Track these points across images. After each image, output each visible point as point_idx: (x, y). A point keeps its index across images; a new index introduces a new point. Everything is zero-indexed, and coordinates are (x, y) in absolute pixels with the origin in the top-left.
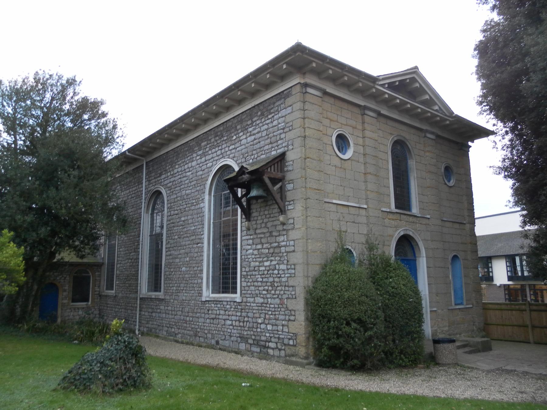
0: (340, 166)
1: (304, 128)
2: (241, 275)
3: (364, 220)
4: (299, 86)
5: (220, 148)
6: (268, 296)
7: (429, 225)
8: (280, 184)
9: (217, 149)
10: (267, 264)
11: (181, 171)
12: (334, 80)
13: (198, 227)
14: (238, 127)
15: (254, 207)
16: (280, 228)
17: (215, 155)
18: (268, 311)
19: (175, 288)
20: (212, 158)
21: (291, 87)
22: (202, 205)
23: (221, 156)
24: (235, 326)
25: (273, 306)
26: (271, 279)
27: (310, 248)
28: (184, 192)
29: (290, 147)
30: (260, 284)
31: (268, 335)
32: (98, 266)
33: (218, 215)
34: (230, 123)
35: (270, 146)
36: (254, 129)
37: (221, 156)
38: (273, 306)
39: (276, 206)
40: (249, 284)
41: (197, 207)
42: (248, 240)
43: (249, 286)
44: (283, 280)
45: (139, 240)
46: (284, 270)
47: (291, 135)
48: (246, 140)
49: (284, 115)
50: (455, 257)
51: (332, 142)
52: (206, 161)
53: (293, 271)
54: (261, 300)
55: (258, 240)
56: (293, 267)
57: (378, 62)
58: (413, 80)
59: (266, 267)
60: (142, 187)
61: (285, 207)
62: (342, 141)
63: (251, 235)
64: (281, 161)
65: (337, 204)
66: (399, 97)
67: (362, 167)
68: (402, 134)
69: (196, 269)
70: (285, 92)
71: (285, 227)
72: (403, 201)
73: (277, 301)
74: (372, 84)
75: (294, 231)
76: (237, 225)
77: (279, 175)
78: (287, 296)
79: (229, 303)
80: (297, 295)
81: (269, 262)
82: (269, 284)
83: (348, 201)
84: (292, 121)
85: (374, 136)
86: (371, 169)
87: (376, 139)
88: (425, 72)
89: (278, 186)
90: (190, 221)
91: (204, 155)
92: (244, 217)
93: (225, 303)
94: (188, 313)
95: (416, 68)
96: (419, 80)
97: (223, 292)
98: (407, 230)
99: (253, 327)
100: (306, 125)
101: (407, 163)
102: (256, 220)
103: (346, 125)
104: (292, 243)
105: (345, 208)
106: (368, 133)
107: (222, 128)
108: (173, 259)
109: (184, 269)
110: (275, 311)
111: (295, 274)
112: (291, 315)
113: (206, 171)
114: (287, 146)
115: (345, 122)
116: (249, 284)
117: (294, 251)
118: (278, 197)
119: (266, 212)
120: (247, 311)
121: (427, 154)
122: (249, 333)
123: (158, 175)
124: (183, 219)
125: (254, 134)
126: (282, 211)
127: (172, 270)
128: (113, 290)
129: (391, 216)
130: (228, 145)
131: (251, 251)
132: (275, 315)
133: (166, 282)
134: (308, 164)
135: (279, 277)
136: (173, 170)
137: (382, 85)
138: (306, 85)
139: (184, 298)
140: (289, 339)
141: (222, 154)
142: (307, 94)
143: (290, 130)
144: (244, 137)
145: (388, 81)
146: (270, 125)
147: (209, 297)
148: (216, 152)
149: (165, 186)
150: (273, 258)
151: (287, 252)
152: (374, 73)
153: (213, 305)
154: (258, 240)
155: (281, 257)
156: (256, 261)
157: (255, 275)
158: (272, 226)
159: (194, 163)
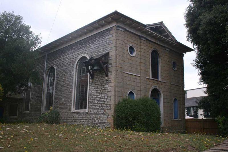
1: (117, 43)
2: (89, 101)
3: (139, 81)
4: (115, 27)
5: (82, 49)
6: (100, 109)
7: (165, 85)
8: (106, 65)
9: (80, 50)
10: (99, 96)
11: (64, 58)
12: (129, 25)
13: (71, 82)
14: (90, 41)
15: (95, 73)
16: (106, 82)
17: (79, 52)
18: (99, 115)
19: (58, 108)
20: (78, 53)
21: (112, 27)
22: (72, 73)
23: (82, 53)
24: (85, 122)
25: (101, 113)
26: (101, 102)
27: (117, 90)
28: (64, 68)
29: (111, 50)
30: (96, 104)
31: (99, 124)
32: (22, 100)
33: (79, 77)
34: (86, 40)
35: (103, 49)
36: (97, 43)
37: (82, 53)
38: (101, 113)
39: (104, 73)
40: (92, 105)
41: (70, 74)
42: (92, 87)
43: (92, 106)
44: (106, 102)
45: (42, 88)
46: (106, 99)
47: (111, 46)
48: (93, 47)
49: (109, 37)
50: (175, 100)
51: (127, 49)
52: (75, 55)
53: (110, 99)
54: (97, 111)
55: (97, 87)
56: (110, 97)
57: (147, 19)
58: (161, 27)
59: (99, 97)
60: (45, 65)
61: (108, 74)
62: (132, 49)
63: (93, 85)
64: (107, 56)
65: (129, 76)
66: (155, 34)
67: (139, 60)
68: (156, 48)
69: (69, 99)
70: (110, 29)
71: (108, 82)
72: (155, 74)
73: (103, 111)
74: (144, 28)
75: (111, 83)
76: (87, 81)
77: (106, 61)
78: (107, 109)
79: (83, 113)
80: (111, 108)
81: (100, 96)
82: (100, 104)
83: (133, 73)
84: (112, 40)
85: (145, 48)
86: (143, 61)
87: (145, 49)
88: (165, 23)
89: (105, 65)
90: (67, 80)
91: (74, 52)
92: (91, 78)
93: (81, 113)
94: (64, 118)
96: (163, 27)
97: (80, 109)
98: (156, 86)
99: (93, 122)
100: (118, 42)
101: (157, 60)
102: (96, 79)
103: (134, 43)
104: (110, 88)
106: (142, 47)
107: (83, 41)
108: (58, 96)
109: (63, 100)
110: (102, 115)
111: (110, 100)
112: (109, 116)
113: (75, 59)
114: (110, 50)
115: (133, 42)
116: (92, 105)
117: (111, 91)
118: (105, 70)
119: (100, 76)
120: (91, 115)
121: (166, 57)
122: (91, 124)
123: (53, 60)
124: (63, 79)
125: (96, 45)
126: (107, 75)
127: (58, 100)
128: (28, 111)
129: (150, 81)
130: (85, 48)
131: (93, 91)
132: (102, 116)
133: (55, 106)
134: (118, 57)
135: (104, 102)
136: (60, 58)
137: (148, 28)
138: (118, 27)
139: (63, 112)
140: (107, 125)
141: (82, 52)
142: (118, 30)
143: (111, 44)
144: (92, 45)
145: (150, 27)
146: (103, 41)
147: (74, 111)
148: (80, 51)
149: (56, 65)
150: (102, 94)
151: (108, 91)
152: (145, 23)
153: (76, 114)
154: (97, 87)
155: (105, 93)
156: (95, 95)
157: (94, 101)
158: (102, 81)
159: (69, 55)
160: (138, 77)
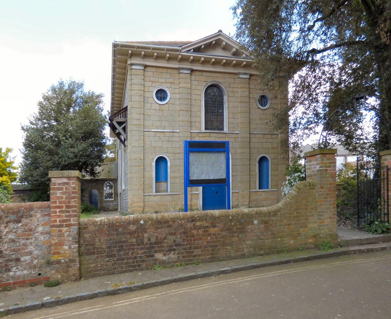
0: (159, 109)
62: (161, 94)
64: (125, 111)
68: (216, 80)
83: (157, 129)
95: (220, 31)
103: (166, 83)
105: (162, 133)
129: (201, 135)
160: (175, 134)
